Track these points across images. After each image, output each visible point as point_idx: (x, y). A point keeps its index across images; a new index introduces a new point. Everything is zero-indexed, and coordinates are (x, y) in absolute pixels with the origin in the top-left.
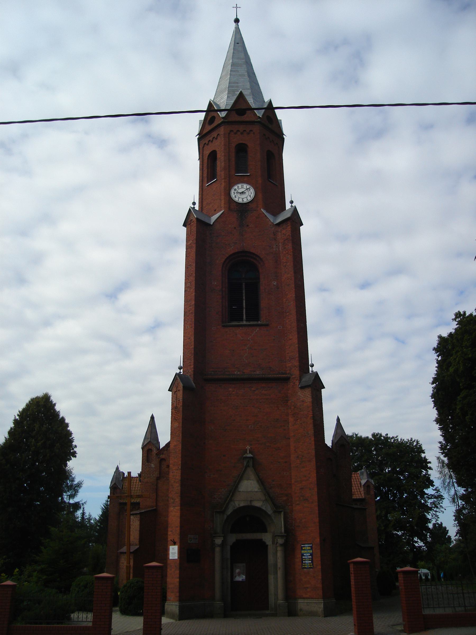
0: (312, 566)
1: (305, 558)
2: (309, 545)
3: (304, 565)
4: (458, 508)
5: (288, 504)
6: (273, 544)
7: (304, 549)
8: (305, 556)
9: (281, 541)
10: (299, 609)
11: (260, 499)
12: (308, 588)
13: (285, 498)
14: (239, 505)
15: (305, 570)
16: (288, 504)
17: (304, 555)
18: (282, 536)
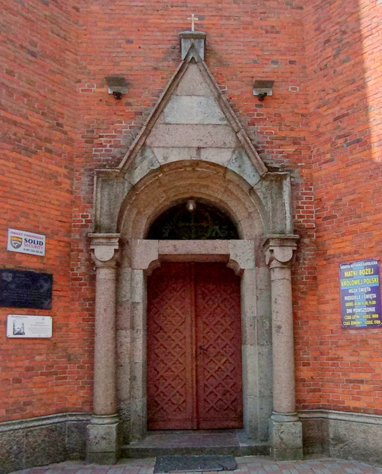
0: (378, 322)
1: (353, 301)
2: (369, 264)
3: (350, 314)
4: (347, 305)
5: (299, 164)
6: (257, 265)
7: (350, 275)
8: (352, 294)
9: (284, 254)
10: (331, 436)
11: (225, 143)
12: (362, 382)
13: (291, 149)
14: (165, 158)
15: (353, 332)
16: (299, 164)
17: (350, 291)
18: (283, 242)
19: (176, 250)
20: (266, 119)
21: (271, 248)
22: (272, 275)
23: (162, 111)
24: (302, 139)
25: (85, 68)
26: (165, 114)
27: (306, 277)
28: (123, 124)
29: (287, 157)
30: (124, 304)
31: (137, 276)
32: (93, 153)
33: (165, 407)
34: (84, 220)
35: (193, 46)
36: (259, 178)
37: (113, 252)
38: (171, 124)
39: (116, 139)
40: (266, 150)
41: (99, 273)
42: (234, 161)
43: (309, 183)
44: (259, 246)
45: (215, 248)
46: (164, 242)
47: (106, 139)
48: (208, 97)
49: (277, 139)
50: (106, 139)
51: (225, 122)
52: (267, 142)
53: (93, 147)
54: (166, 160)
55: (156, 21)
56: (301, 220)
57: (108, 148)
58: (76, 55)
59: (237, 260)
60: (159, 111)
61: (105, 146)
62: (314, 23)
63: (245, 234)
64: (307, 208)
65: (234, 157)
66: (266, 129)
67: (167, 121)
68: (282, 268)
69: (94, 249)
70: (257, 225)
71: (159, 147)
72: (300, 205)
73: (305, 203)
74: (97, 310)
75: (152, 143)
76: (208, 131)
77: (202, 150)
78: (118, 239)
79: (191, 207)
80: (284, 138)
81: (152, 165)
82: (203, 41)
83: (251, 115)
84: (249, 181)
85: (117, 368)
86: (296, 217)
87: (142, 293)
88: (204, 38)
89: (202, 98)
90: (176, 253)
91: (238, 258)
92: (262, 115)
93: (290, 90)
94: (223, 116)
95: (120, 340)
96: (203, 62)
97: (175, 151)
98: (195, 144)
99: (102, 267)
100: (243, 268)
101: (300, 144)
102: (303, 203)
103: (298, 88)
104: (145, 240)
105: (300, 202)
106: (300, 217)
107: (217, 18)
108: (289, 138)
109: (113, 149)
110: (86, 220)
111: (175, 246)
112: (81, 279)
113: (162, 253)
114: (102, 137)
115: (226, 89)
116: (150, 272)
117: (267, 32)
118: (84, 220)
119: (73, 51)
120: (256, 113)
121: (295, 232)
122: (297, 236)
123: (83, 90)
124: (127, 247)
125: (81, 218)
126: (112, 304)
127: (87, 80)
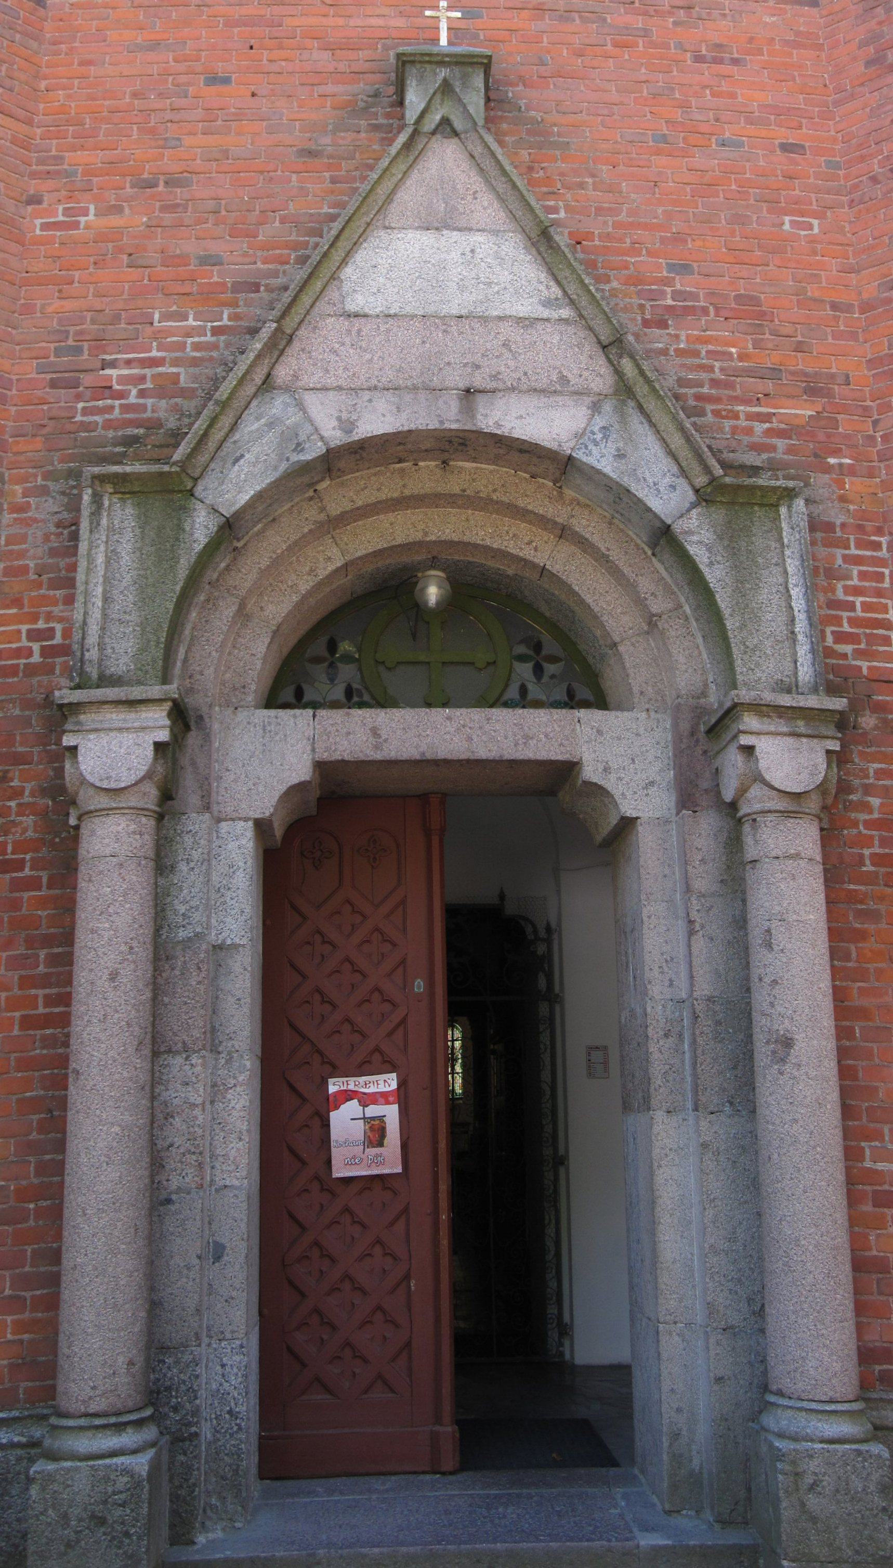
5: (832, 461)
16: (832, 461)
19: (377, 747)
20: (705, 311)
21: (745, 740)
22: (748, 840)
23: (334, 277)
24: (841, 380)
25: (59, 159)
26: (346, 287)
27: (873, 855)
28: (191, 322)
29: (781, 434)
30: (178, 952)
31: (232, 846)
32: (79, 418)
33: (230, 902)
34: (36, 647)
35: (446, 88)
36: (691, 496)
37: (150, 752)
38: (366, 316)
39: (161, 369)
40: (709, 407)
41: (93, 833)
42: (599, 436)
43: (869, 525)
44: (692, 734)
45: (527, 738)
46: (331, 718)
47: (126, 372)
48: (495, 233)
49: (749, 373)
50: (126, 372)
51: (566, 313)
52: (714, 383)
53: (79, 397)
54: (349, 432)
55: (312, 21)
56: (848, 649)
57: (132, 399)
58: (29, 123)
59: (609, 784)
60: (325, 273)
61: (121, 395)
62: (863, 44)
63: (636, 690)
64: (866, 607)
65: (599, 421)
66: (707, 340)
67: (351, 307)
68: (787, 814)
69: (75, 748)
70: (682, 659)
71: (325, 389)
72: (840, 594)
73: (857, 591)
74: (82, 977)
75: (296, 377)
76: (502, 338)
77: (481, 400)
78: (170, 704)
79: (433, 593)
80: (775, 373)
81: (299, 448)
82: (478, 81)
83: (653, 296)
84: (655, 504)
85: (152, 1209)
86: (830, 639)
87: (248, 910)
88: (486, 64)
89: (479, 238)
90: (379, 756)
91: (613, 777)
92: (694, 296)
93: (787, 227)
94: (556, 291)
95: (165, 1095)
96: (482, 132)
97: (382, 403)
98: (457, 379)
99: (107, 811)
100: (630, 813)
101: (829, 394)
102: (848, 590)
103: (815, 222)
104: (266, 712)
105: (839, 586)
106: (840, 638)
107: (525, 14)
108: (793, 373)
109: (149, 402)
110: (43, 648)
111: (375, 732)
112: (19, 865)
113: (325, 756)
114: (113, 364)
115: (562, 214)
116: (279, 832)
117: (699, 59)
118: (36, 647)
119: (21, 113)
120: (669, 290)
121: (832, 690)
122: (838, 704)
123: (45, 226)
124: (193, 739)
125: (25, 643)
126: (143, 953)
127: (64, 193)
